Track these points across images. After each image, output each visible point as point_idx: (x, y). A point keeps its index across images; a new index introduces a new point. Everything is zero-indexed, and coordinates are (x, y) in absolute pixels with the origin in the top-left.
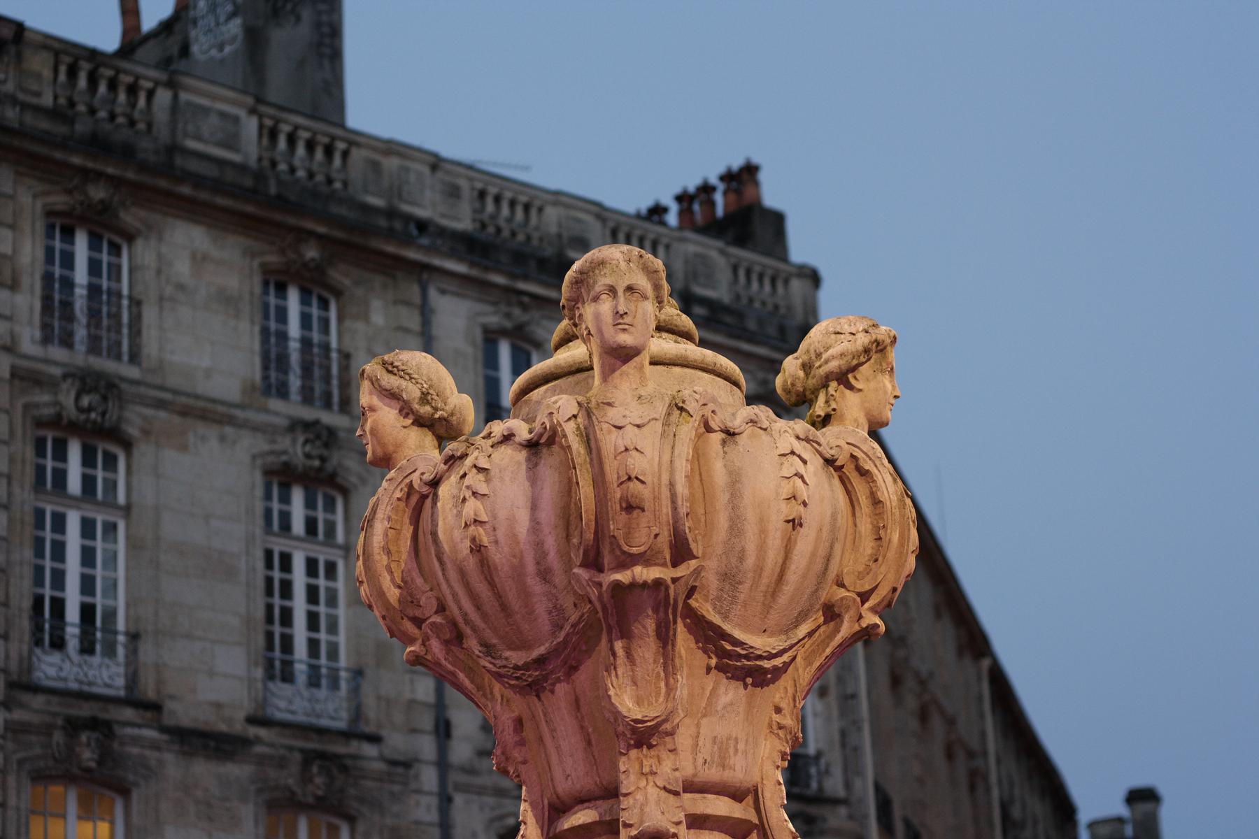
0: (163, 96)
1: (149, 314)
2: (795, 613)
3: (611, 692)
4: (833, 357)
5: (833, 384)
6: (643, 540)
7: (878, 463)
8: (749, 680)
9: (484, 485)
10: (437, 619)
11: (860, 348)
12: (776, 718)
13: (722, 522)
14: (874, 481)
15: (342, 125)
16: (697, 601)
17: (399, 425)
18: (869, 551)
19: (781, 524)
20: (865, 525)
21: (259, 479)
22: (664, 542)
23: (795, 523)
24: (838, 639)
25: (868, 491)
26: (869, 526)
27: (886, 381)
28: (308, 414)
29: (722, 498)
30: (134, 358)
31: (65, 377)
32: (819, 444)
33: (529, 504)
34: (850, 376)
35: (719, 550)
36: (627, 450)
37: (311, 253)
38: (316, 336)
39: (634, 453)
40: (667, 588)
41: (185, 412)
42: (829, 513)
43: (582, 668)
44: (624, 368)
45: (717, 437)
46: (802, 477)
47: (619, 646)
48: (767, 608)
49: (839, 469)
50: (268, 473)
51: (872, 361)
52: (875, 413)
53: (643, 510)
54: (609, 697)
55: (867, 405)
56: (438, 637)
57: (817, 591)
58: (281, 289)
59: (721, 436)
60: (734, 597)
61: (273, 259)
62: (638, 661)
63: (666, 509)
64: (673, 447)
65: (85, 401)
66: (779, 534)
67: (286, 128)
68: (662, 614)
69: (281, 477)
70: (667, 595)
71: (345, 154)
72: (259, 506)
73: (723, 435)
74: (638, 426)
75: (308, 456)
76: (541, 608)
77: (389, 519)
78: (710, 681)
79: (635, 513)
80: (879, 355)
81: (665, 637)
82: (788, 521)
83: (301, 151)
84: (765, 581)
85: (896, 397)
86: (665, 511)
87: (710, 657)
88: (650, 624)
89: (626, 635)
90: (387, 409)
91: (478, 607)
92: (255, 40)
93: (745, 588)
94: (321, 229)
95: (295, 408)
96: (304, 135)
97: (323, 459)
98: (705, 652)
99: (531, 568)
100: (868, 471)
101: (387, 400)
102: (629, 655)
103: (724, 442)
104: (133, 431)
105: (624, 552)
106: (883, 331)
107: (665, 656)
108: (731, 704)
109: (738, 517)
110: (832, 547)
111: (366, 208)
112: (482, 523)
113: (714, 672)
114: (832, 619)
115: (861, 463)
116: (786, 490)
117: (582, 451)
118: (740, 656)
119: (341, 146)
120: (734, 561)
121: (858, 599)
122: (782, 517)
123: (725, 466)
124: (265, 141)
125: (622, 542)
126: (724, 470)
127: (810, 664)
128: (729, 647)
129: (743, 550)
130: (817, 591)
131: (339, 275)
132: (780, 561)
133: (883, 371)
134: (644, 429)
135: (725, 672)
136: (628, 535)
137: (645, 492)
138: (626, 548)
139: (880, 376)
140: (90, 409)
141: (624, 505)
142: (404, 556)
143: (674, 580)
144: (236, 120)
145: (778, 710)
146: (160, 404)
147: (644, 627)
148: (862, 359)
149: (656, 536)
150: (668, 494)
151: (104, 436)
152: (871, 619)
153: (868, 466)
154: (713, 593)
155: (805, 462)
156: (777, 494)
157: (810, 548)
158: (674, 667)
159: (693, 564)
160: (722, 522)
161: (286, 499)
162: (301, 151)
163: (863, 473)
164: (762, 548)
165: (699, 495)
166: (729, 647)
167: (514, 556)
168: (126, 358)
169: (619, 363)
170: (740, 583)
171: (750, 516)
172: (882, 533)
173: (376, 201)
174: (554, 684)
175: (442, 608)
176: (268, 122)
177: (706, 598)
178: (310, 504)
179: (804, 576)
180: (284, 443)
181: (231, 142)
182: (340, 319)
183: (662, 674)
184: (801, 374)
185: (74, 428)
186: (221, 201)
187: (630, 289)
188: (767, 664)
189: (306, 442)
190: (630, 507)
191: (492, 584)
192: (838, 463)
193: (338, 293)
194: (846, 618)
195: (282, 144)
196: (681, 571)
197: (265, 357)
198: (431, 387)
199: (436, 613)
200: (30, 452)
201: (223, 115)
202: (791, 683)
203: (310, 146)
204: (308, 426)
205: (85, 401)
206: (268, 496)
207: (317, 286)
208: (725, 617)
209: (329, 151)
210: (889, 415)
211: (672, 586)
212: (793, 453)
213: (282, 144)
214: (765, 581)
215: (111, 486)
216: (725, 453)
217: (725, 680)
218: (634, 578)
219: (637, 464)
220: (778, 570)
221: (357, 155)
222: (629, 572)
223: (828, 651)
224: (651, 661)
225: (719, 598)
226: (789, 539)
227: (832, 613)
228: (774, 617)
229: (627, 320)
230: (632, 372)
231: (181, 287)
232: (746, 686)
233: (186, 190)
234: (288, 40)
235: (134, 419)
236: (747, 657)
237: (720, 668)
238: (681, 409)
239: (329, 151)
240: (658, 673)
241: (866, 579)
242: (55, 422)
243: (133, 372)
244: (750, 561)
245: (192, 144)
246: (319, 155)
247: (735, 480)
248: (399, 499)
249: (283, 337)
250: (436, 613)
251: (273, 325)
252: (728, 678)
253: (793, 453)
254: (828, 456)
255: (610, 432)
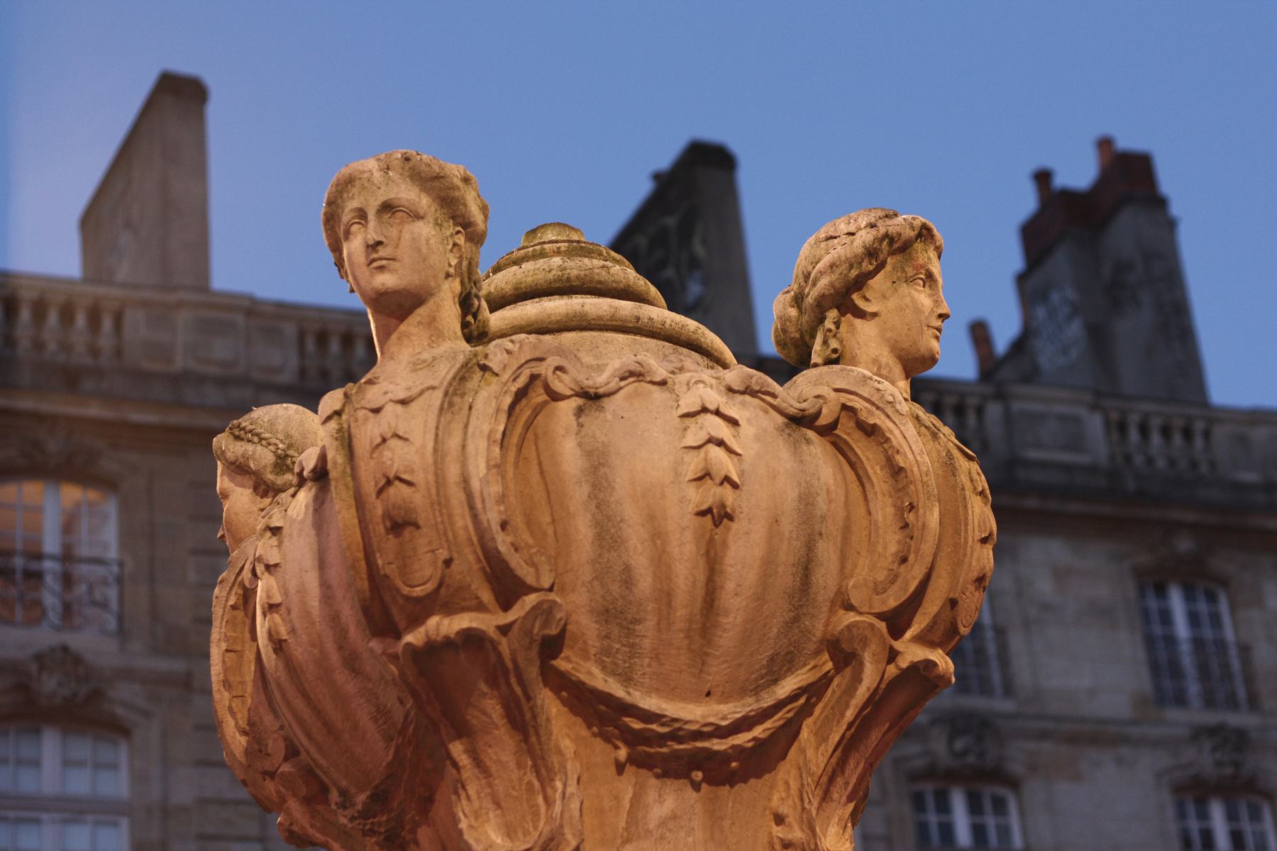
0: (994, 411)
1: (1016, 642)
2: (763, 658)
3: (463, 825)
4: (821, 273)
5: (832, 314)
6: (428, 572)
7: (889, 411)
8: (697, 775)
9: (275, 551)
10: (286, 768)
11: (860, 251)
12: (778, 831)
13: (583, 529)
14: (888, 440)
15: (1204, 403)
16: (568, 659)
17: (255, 509)
18: (893, 548)
19: (689, 520)
20: (883, 510)
21: (1167, 798)
22: (468, 567)
23: (718, 516)
24: (862, 693)
25: (882, 457)
26: (890, 510)
27: (923, 298)
28: (1211, 718)
29: (578, 494)
30: (1009, 689)
31: (934, 722)
32: (774, 396)
33: (316, 562)
34: (854, 296)
35: (586, 574)
36: (384, 440)
37: (1184, 545)
38: (1208, 633)
39: (393, 443)
40: (495, 645)
41: (1073, 739)
42: (792, 494)
43: (437, 797)
44: (403, 327)
45: (567, 407)
46: (721, 443)
47: (457, 749)
48: (700, 658)
49: (827, 431)
50: (1179, 790)
51: (888, 268)
52: (906, 345)
53: (418, 527)
54: (461, 832)
55: (889, 335)
56: (295, 795)
57: (796, 619)
58: (1161, 590)
59: (576, 402)
60: (633, 646)
61: (1144, 559)
62: (493, 769)
63: (462, 521)
64: (466, 426)
65: (959, 745)
66: (688, 535)
67: (1134, 419)
68: (504, 688)
69: (1193, 792)
70: (499, 655)
71: (1207, 434)
72: (1173, 828)
73: (579, 401)
74: (403, 402)
75: (1219, 764)
76: (364, 715)
77: (227, 639)
78: (626, 787)
79: (408, 532)
80: (899, 257)
81: (523, 723)
82: (702, 514)
83: (1156, 439)
84: (680, 613)
85: (943, 317)
86: (460, 523)
87: (617, 748)
88: (493, 707)
89: (463, 731)
90: (239, 490)
91: (309, 736)
92: (1099, 337)
93: (648, 627)
94: (1190, 517)
95: (1199, 715)
96: (1156, 423)
97: (1237, 765)
98: (607, 739)
99: (335, 658)
100: (874, 425)
101: (239, 478)
102: (478, 762)
103: (580, 411)
104: (1016, 768)
105: (408, 598)
106: (901, 224)
107: (531, 752)
108: (674, 817)
109: (609, 518)
110: (810, 547)
111: (1239, 487)
112: (278, 605)
113: (630, 770)
114: (847, 664)
115: (863, 416)
116: (693, 464)
117: (340, 460)
118: (662, 739)
119: (1199, 426)
120: (615, 588)
121: (882, 626)
122: (692, 508)
123: (580, 445)
124: (1115, 436)
125: (399, 583)
126: (578, 451)
127: (825, 740)
128: (637, 725)
129: (627, 569)
130: (796, 619)
131: (1221, 563)
132: (701, 578)
133: (910, 280)
134: (414, 406)
135: (650, 767)
136: (404, 569)
137: (417, 498)
138: (405, 590)
139: (904, 288)
140: (965, 753)
141: (388, 524)
142: (249, 688)
143: (504, 630)
144: (1076, 420)
145: (779, 820)
146: (1044, 735)
147: (484, 713)
148: (867, 266)
149: (448, 563)
150: (463, 497)
151: (987, 780)
152: (911, 652)
153: (878, 419)
154: (594, 644)
155: (734, 422)
156: (677, 474)
157: (758, 552)
158: (549, 770)
159: (531, 600)
160: (583, 529)
161: (1203, 815)
162: (1156, 439)
163: (871, 431)
164: (661, 562)
165: (540, 495)
166: (637, 725)
167: (313, 645)
168: (999, 690)
169: (394, 321)
170: (637, 621)
171: (631, 515)
172: (911, 517)
173: (1250, 477)
174: (413, 831)
175: (292, 752)
176: (1114, 416)
177: (585, 655)
178: (1232, 816)
179: (760, 598)
180: (1189, 754)
181: (1076, 443)
182: (1233, 609)
183: (537, 784)
184: (793, 312)
185: (951, 776)
186: (1075, 507)
187: (388, 208)
188: (718, 745)
189: (1214, 749)
190: (400, 524)
191: (306, 696)
192: (822, 421)
193: (1224, 583)
194: (867, 658)
195: (1134, 435)
196: (516, 613)
197: (1154, 667)
198: (290, 446)
199: (286, 759)
200: (907, 810)
201: (1063, 418)
202: (794, 772)
203: (1166, 432)
204: (1214, 731)
205: (959, 745)
206: (1182, 815)
207: (1199, 580)
208: (627, 679)
209: (1188, 434)
210: (935, 345)
211: (504, 640)
212: (705, 410)
213: (1134, 435)
214: (680, 613)
215: (1004, 832)
216: (581, 425)
217: (653, 781)
218: (427, 635)
219: (398, 457)
220: (700, 593)
221: (1220, 433)
222: (422, 630)
223: (850, 714)
224: (512, 765)
225: (606, 651)
226: (711, 541)
227: (843, 654)
228: (717, 672)
229: (382, 252)
230: (414, 330)
231: (1046, 607)
232: (696, 787)
233: (1032, 503)
234: (1132, 328)
235: (1016, 756)
236: (675, 736)
237: (639, 761)
238: (484, 368)
239: (1188, 434)
240: (530, 783)
241: (890, 592)
242: (930, 773)
243: (1003, 705)
244: (645, 584)
245: (1033, 454)
246: (1178, 439)
247: (598, 464)
248: (234, 607)
249: (1171, 640)
250: (286, 759)
251: (1158, 630)
252: (658, 776)
253: (705, 410)
254: (792, 411)
255: (366, 419)
